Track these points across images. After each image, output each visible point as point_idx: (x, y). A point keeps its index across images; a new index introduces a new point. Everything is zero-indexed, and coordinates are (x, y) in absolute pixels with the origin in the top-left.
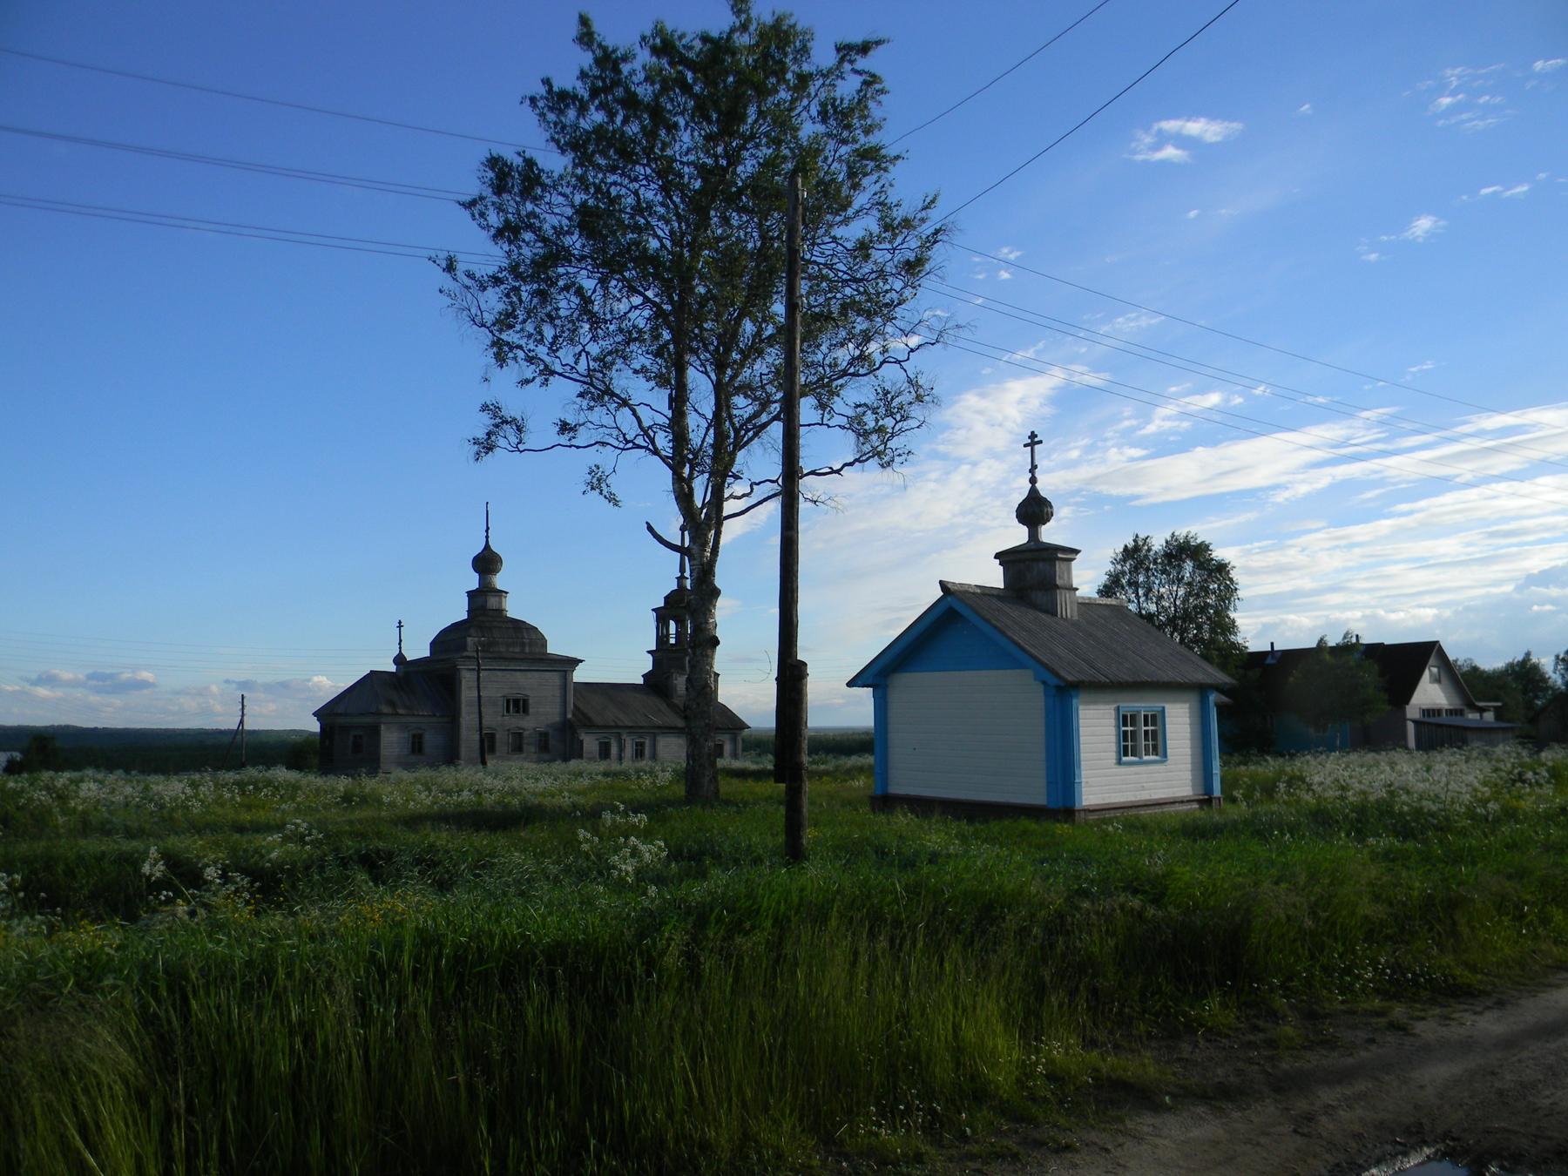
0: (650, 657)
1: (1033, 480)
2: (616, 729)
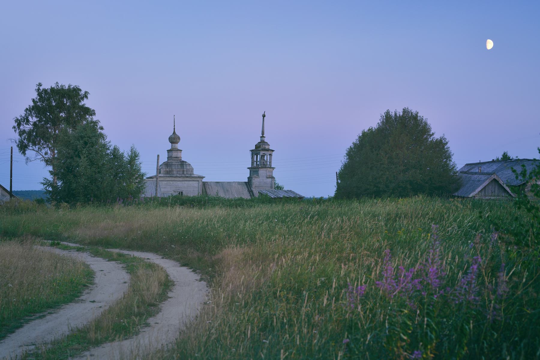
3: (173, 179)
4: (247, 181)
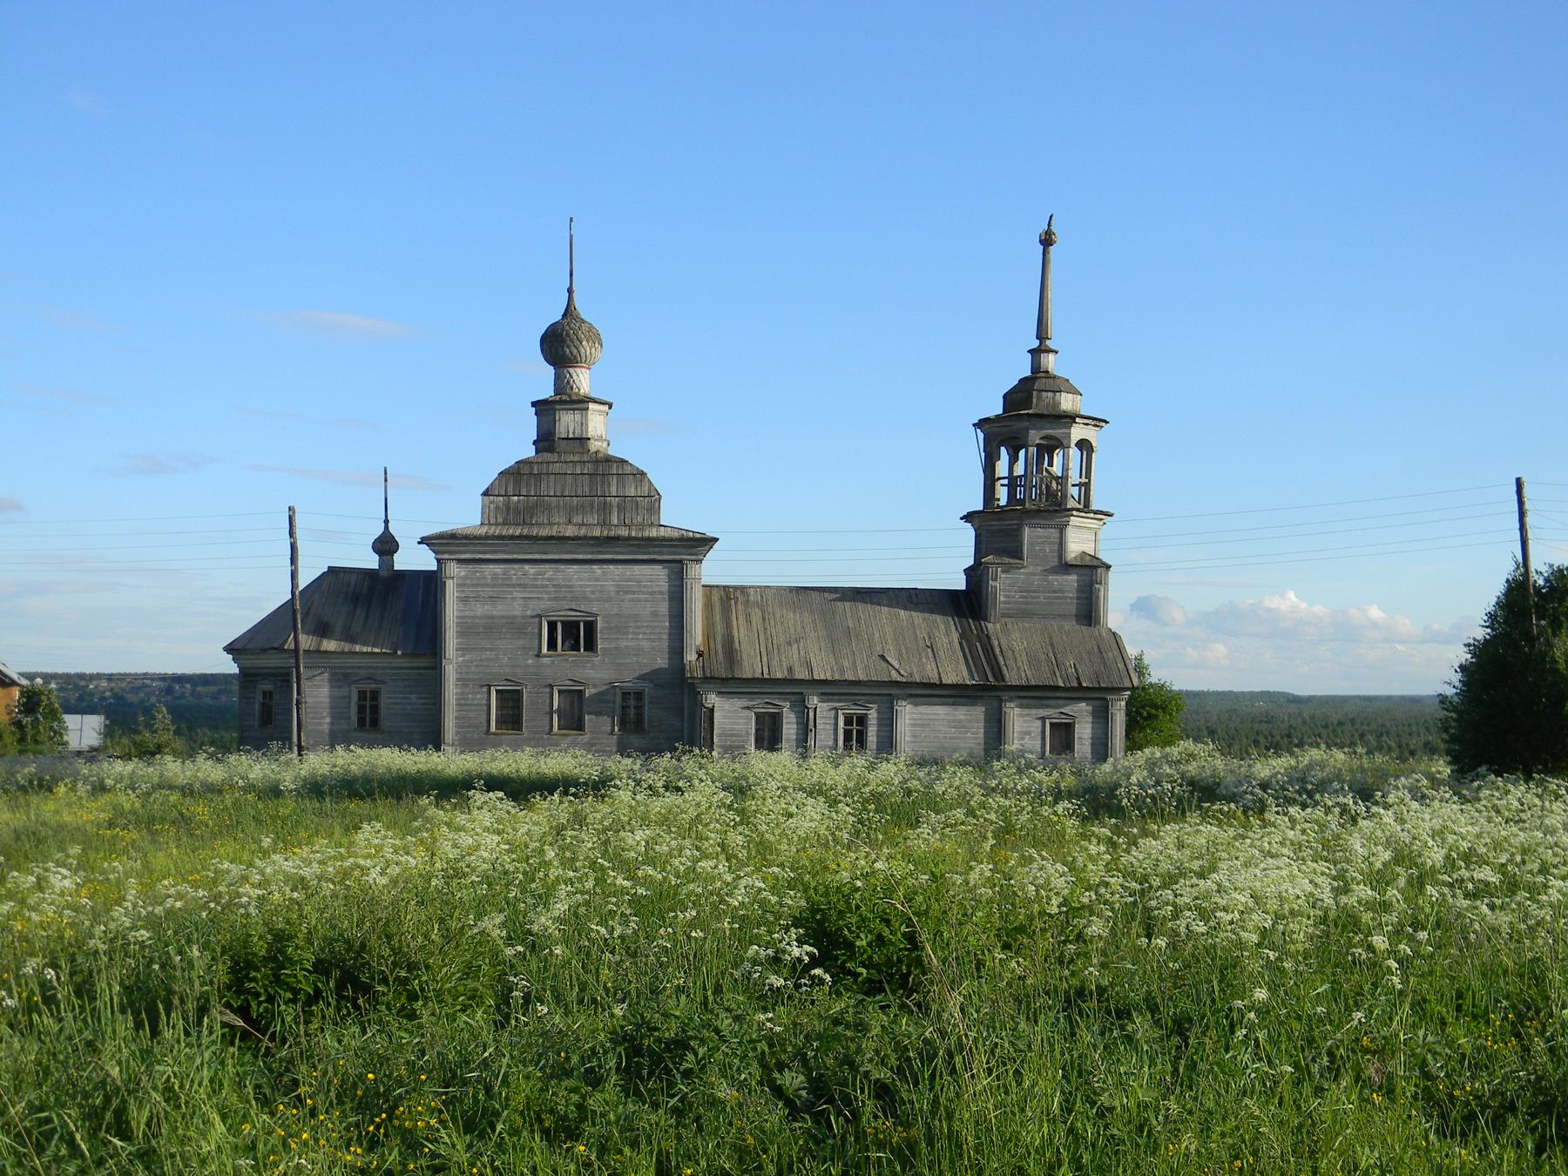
1: (386, 522)
2: (796, 689)
4: (960, 583)
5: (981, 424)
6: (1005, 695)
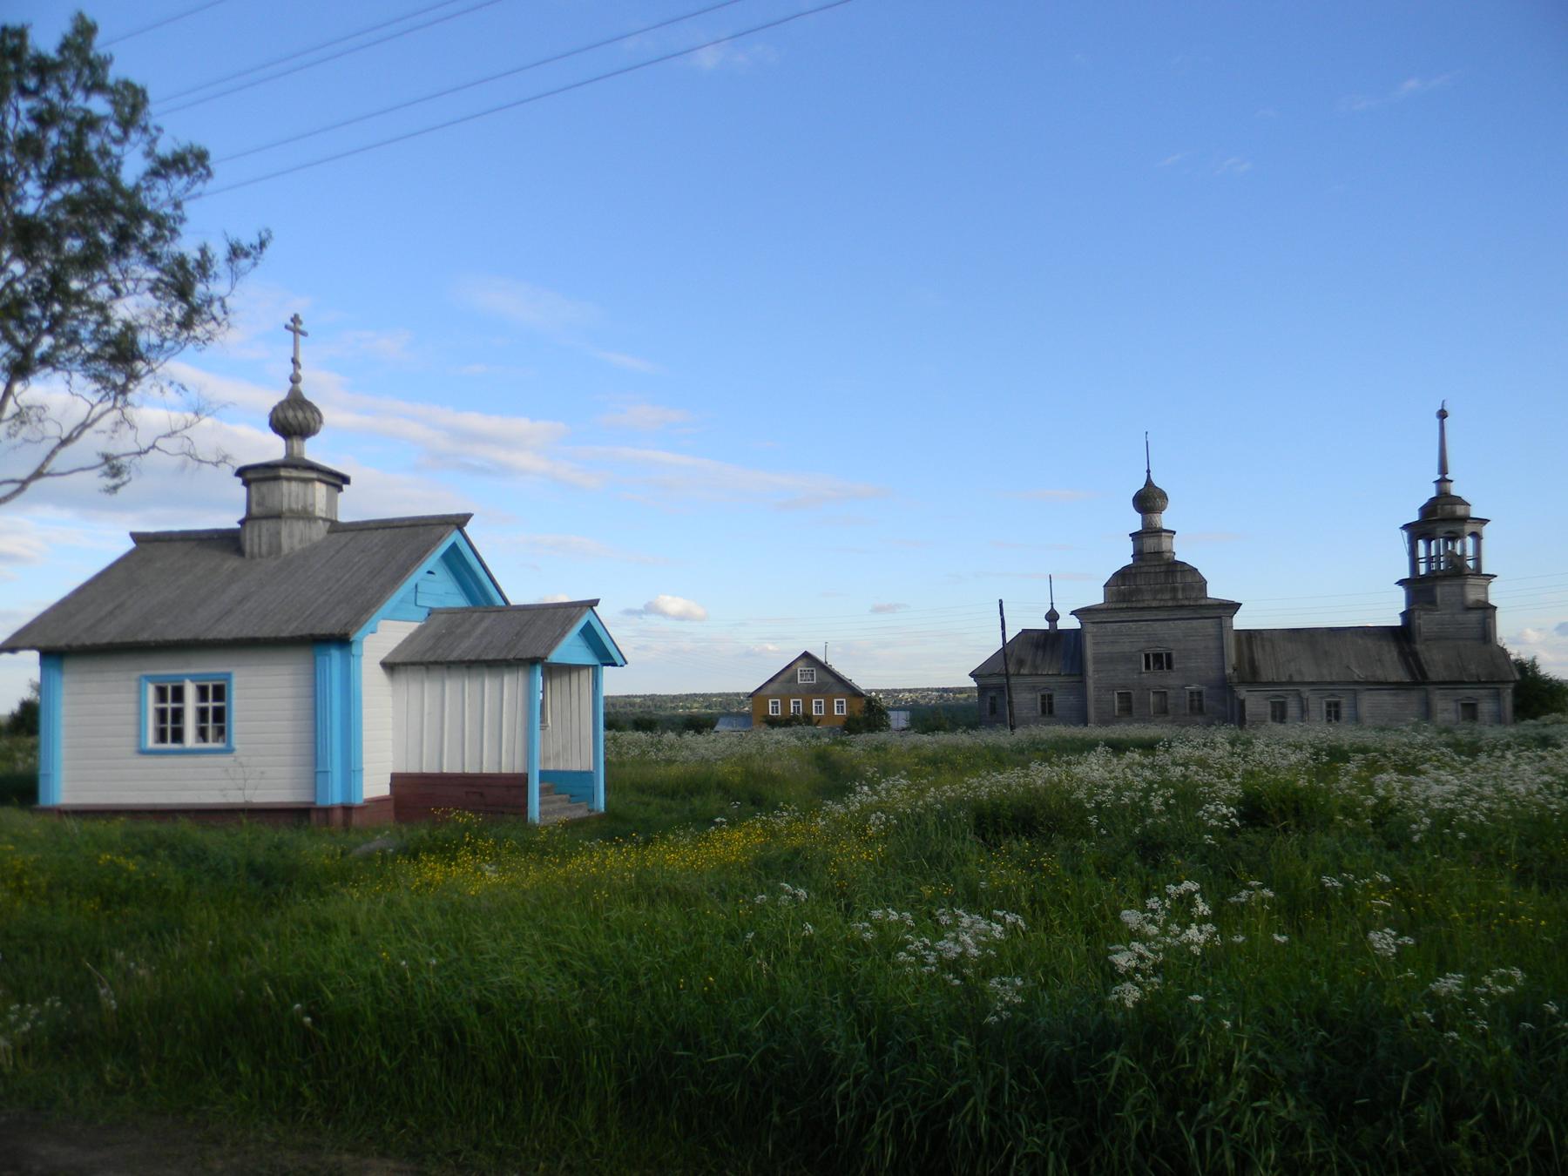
0: (1401, 593)
1: (295, 380)
3: (1136, 615)
5: (1406, 527)
6: (1430, 688)
